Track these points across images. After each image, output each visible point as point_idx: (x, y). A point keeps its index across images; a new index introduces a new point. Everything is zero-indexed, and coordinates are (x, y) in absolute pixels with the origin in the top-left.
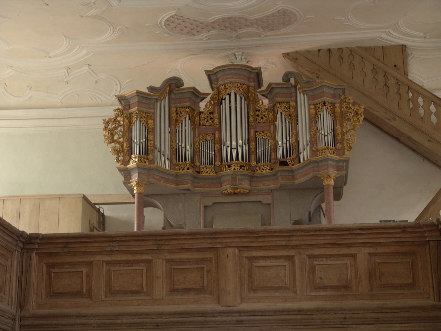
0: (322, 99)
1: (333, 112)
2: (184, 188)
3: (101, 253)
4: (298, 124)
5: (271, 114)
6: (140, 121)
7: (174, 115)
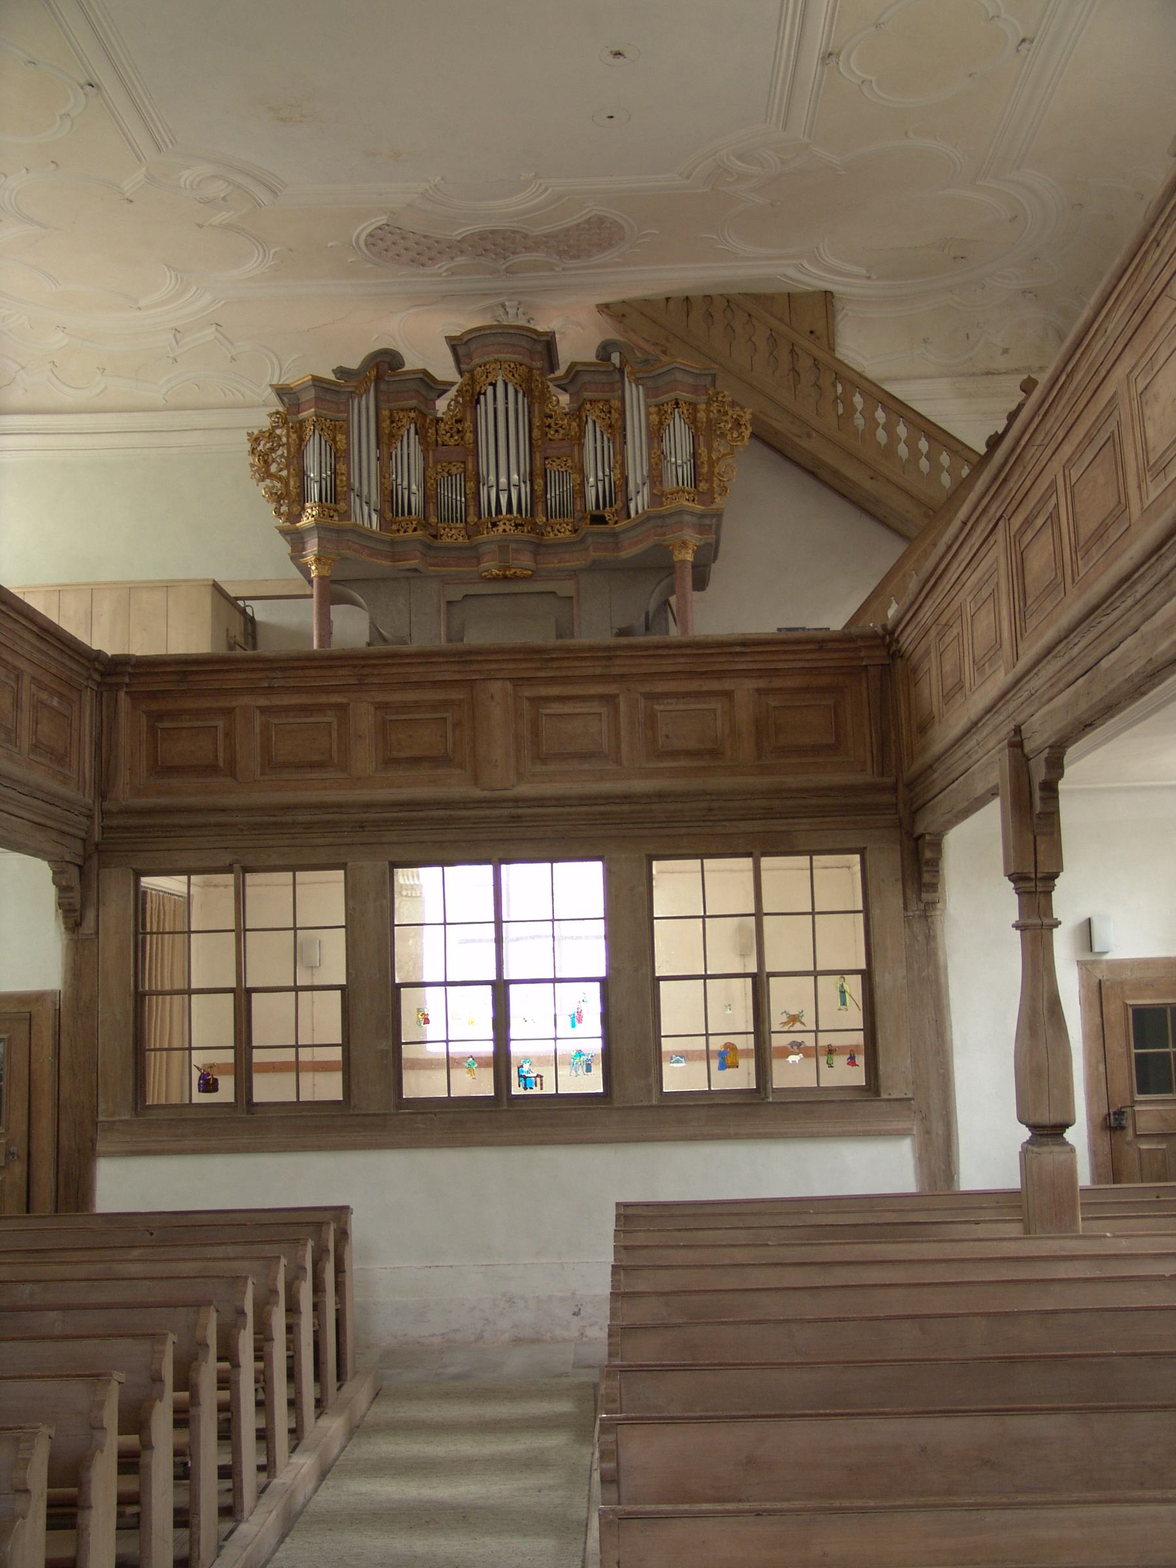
0: (673, 395)
1: (693, 421)
3: (252, 691)
5: (574, 424)
7: (386, 424)
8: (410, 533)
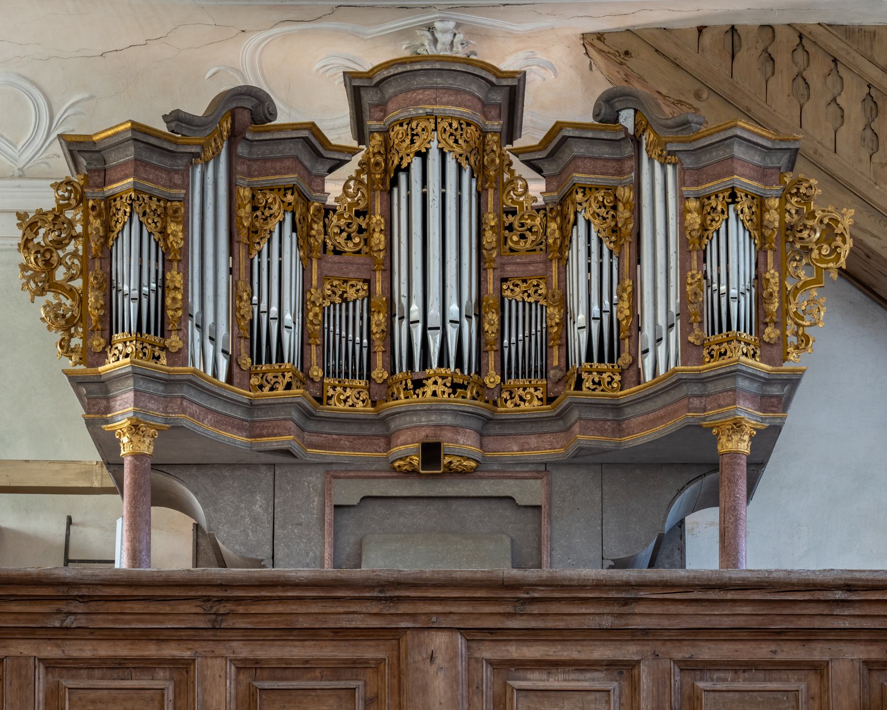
0: (726, 182)
1: (758, 228)
2: (275, 446)
3: (30, 633)
4: (639, 261)
5: (553, 226)
6: (141, 223)
8: (280, 391)
